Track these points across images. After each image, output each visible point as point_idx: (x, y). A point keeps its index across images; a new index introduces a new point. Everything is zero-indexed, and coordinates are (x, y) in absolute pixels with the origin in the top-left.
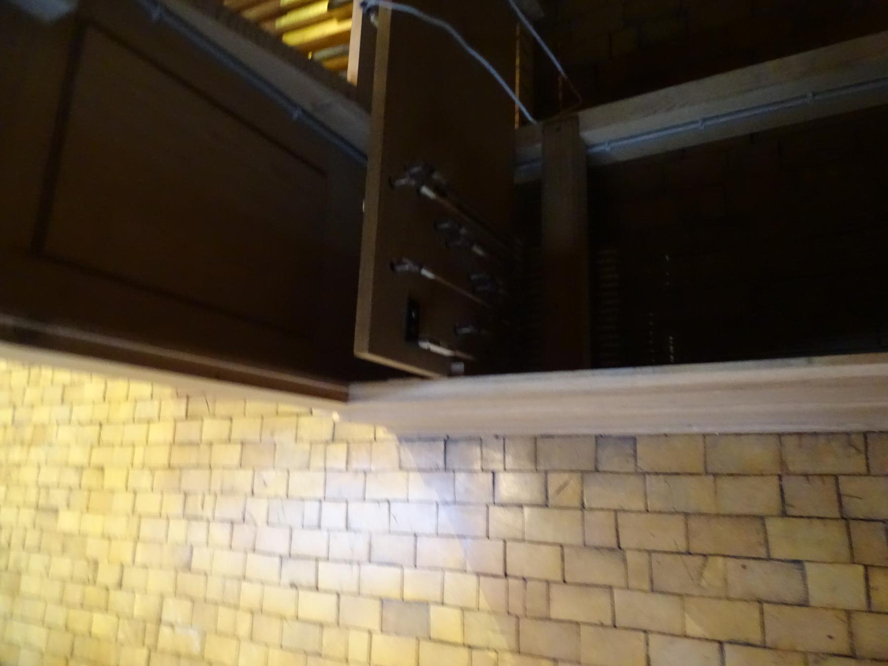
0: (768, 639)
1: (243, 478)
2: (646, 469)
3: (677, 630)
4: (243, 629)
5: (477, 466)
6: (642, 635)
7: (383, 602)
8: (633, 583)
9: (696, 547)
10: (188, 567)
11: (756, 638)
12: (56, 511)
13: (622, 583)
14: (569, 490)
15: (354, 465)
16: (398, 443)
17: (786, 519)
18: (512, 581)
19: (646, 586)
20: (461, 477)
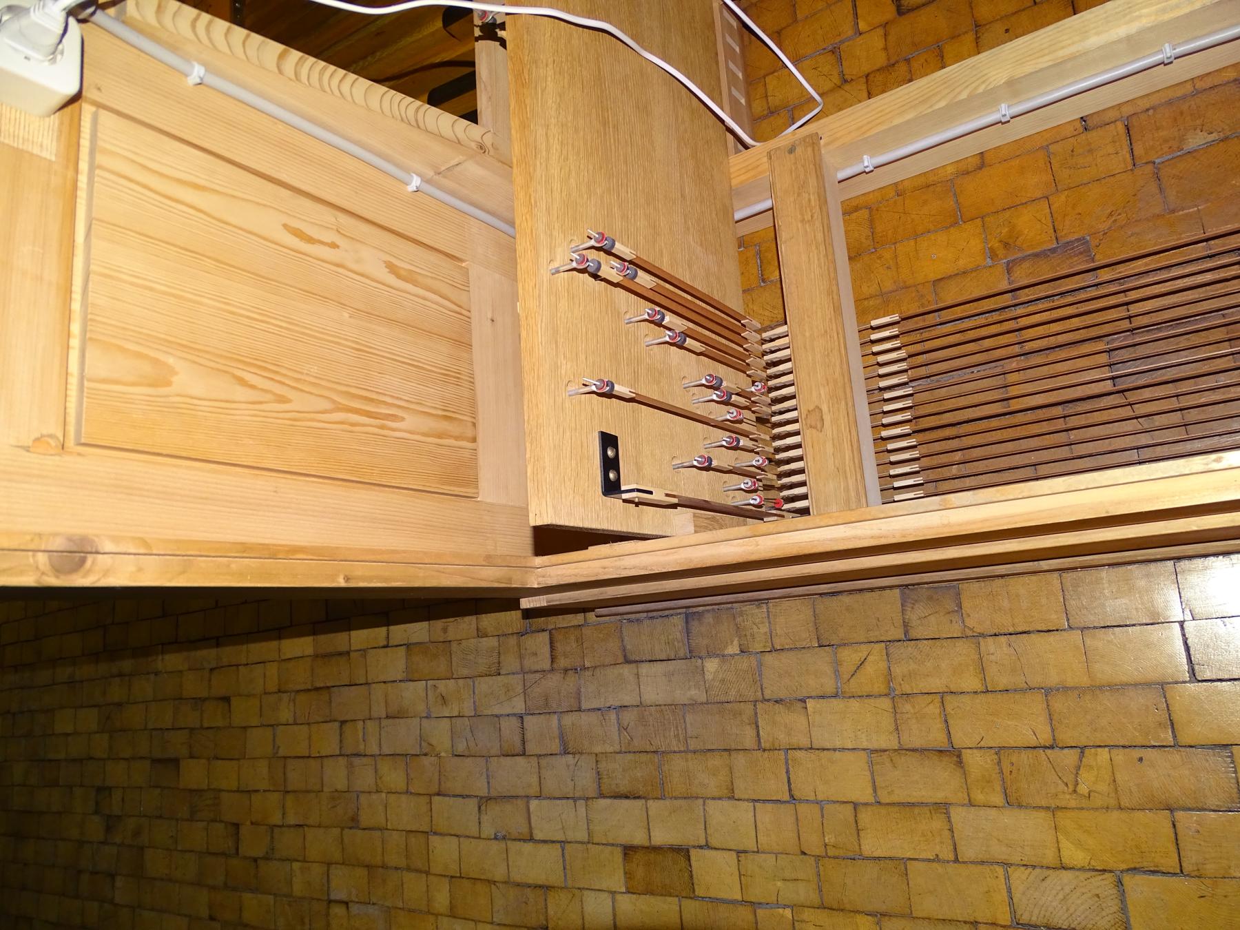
0: (582, 811)
1: (412, 693)
2: (979, 629)
3: (1050, 857)
4: (441, 899)
5: (733, 649)
6: (1000, 870)
7: (629, 851)
8: (979, 797)
9: (1066, 736)
10: (354, 822)
11: (1171, 863)
12: (175, 762)
13: (962, 797)
14: (869, 668)
15: (563, 662)
16: (58, 544)
17: (1153, 676)
18: (802, 808)
19: (998, 799)
20: (711, 665)
